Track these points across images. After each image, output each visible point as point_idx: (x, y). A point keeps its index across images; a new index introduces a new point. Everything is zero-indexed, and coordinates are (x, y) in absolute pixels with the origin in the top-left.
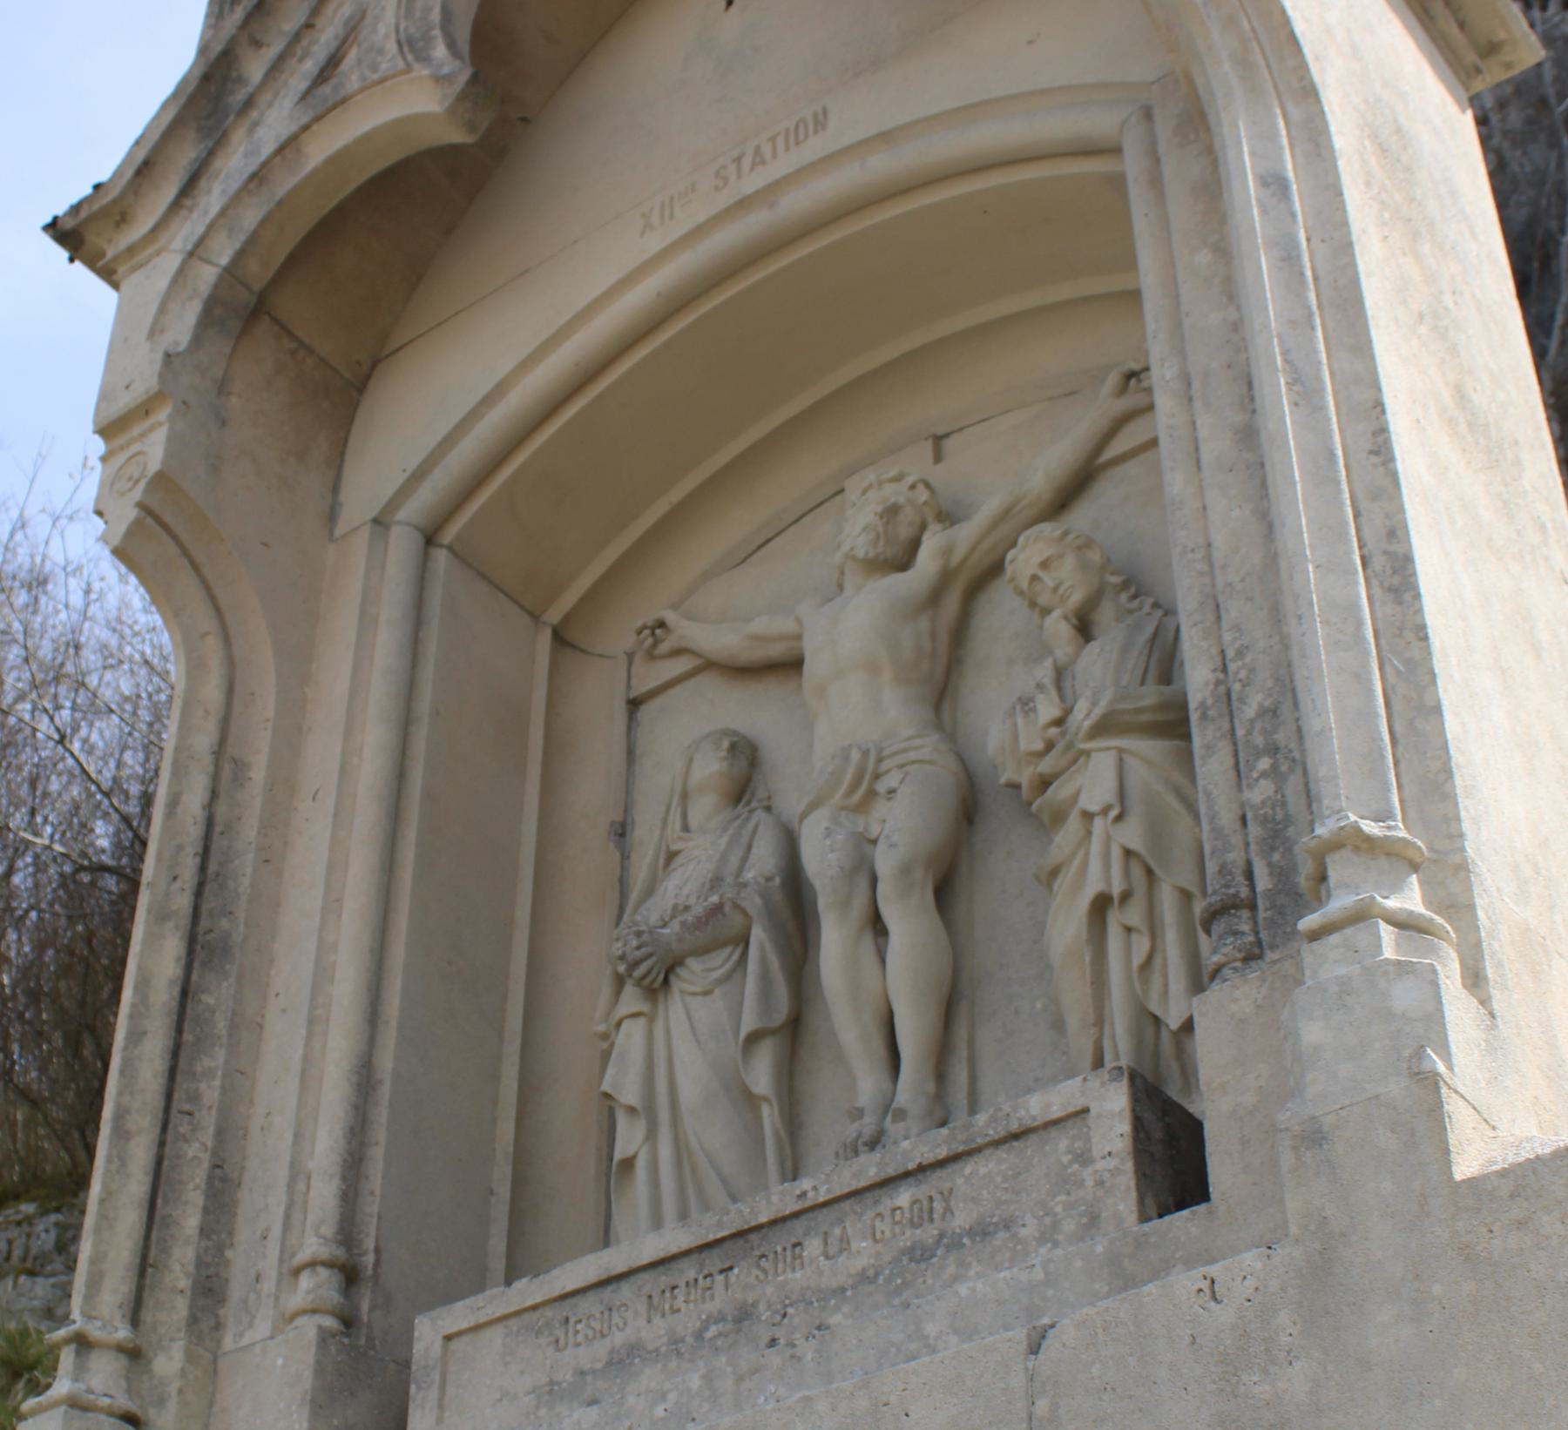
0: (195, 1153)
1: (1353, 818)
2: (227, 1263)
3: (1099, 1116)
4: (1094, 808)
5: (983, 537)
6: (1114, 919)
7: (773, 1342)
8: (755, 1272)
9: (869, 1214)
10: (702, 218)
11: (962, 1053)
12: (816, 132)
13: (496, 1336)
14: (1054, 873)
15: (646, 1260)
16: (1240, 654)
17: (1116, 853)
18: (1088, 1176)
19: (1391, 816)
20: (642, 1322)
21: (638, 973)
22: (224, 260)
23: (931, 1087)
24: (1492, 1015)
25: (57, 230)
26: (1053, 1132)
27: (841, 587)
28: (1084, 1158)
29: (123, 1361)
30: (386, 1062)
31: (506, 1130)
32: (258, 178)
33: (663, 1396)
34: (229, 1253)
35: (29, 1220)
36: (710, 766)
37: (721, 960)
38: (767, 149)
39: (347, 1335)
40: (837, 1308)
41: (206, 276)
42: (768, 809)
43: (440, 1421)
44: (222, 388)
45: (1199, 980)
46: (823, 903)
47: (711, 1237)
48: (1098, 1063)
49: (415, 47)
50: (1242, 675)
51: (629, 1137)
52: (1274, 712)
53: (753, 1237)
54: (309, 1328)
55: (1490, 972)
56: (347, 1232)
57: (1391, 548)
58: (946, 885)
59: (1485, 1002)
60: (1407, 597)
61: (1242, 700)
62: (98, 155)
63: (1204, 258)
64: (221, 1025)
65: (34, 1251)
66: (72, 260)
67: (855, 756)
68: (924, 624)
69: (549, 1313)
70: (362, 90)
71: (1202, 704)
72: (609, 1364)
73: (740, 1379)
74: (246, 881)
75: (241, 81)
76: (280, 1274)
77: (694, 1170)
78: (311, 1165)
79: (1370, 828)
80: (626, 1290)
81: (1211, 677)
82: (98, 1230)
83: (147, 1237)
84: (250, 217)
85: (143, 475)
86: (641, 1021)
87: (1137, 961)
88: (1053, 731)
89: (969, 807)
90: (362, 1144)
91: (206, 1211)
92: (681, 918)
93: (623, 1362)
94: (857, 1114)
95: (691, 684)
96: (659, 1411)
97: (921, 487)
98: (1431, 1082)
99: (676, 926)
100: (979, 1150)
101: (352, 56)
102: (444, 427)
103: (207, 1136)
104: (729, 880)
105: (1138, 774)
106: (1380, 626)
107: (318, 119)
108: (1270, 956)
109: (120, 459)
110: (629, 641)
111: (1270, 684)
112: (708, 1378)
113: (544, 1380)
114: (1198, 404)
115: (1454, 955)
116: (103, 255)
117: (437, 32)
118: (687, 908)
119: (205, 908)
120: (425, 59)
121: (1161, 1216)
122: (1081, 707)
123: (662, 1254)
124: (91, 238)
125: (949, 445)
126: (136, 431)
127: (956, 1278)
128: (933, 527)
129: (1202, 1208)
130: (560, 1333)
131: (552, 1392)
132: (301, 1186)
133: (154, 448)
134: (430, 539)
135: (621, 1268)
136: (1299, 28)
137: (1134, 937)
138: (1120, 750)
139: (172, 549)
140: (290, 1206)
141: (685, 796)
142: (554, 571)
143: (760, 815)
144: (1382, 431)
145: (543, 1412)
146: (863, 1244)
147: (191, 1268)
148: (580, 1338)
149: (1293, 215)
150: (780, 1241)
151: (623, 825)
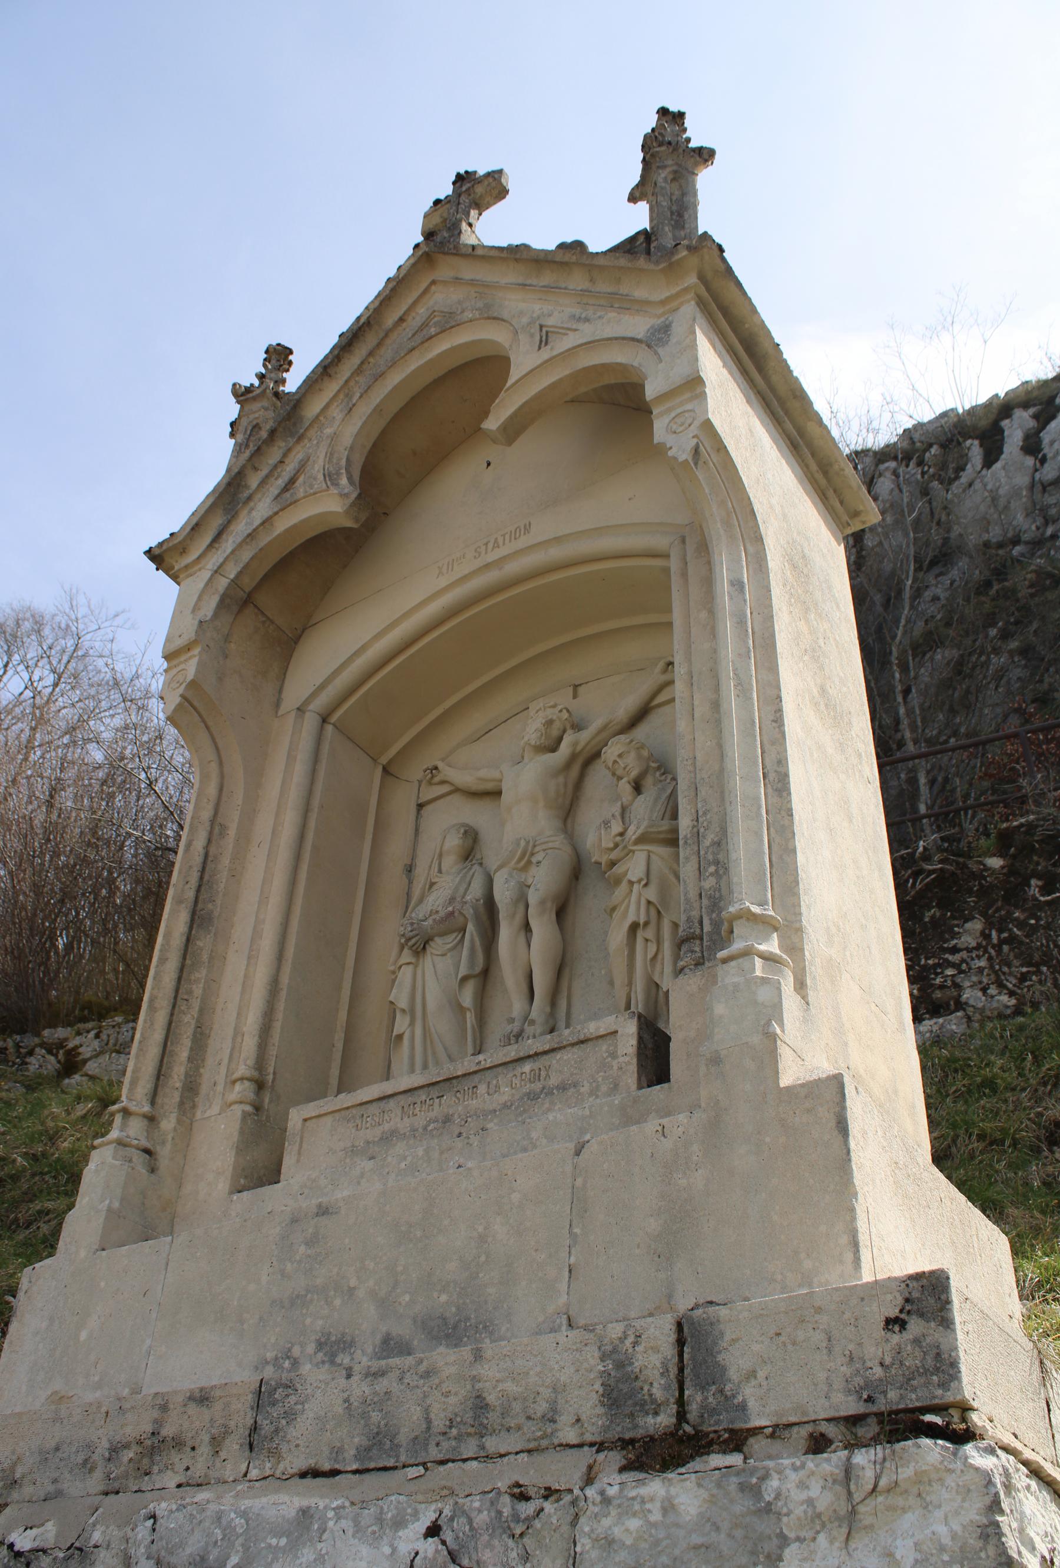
0: (188, 1021)
1: (747, 904)
2: (201, 1075)
3: (622, 1035)
4: (634, 879)
5: (593, 738)
6: (640, 934)
7: (460, 1135)
8: (454, 1099)
9: (510, 1075)
10: (466, 572)
11: (564, 994)
12: (14, 1297)
13: (328, 1120)
14: (614, 909)
15: (402, 1089)
16: (705, 814)
17: (643, 902)
18: (615, 1064)
19: (766, 903)
20: (398, 1119)
21: (410, 944)
22: (232, 576)
23: (548, 1009)
24: (808, 1004)
25: (151, 554)
26: (600, 1041)
27: (523, 757)
28: (613, 1055)
29: (146, 1122)
30: (285, 980)
31: (343, 1015)
32: (251, 536)
33: (405, 1158)
34: (202, 1070)
35: (119, 1025)
36: (454, 841)
37: (451, 939)
38: (500, 540)
39: (257, 1115)
40: (491, 1121)
41: (223, 583)
42: (481, 864)
43: (298, 1161)
44: (227, 639)
45: (679, 972)
46: (502, 915)
47: (434, 1080)
48: (628, 1007)
49: (331, 477)
50: (705, 824)
51: (401, 1024)
52: (719, 844)
53: (454, 1081)
54: (238, 1110)
55: (808, 982)
56: (260, 1063)
57: (779, 770)
58: (562, 911)
59: (804, 997)
60: (784, 794)
61: (704, 837)
62: (170, 518)
63: (704, 615)
64: (205, 957)
65: (120, 1041)
66: (157, 569)
67: (523, 843)
68: (561, 779)
69: (354, 1111)
70: (304, 497)
71: (685, 836)
72: (381, 1139)
73: (442, 1153)
74: (222, 886)
75: (247, 487)
76: (226, 1082)
77: (432, 1042)
78: (245, 1029)
79: (756, 909)
80: (392, 1103)
81: (691, 824)
82: (137, 1056)
83: (162, 1061)
84: (246, 555)
85: (184, 680)
86: (411, 967)
87: (650, 956)
88: (618, 838)
89: (577, 871)
90: (271, 1020)
91: (191, 1049)
92: (433, 917)
93: (388, 1138)
94: (511, 1020)
95: (448, 798)
96: (403, 1165)
97: (565, 711)
98: (773, 1038)
99: (430, 921)
100: (564, 1047)
101: (301, 479)
102: (335, 666)
103: (195, 1012)
104: (459, 899)
105: (657, 864)
106: (770, 808)
107: (282, 510)
108: (707, 964)
109: (174, 671)
110: (420, 775)
111: (718, 829)
112: (427, 1151)
113: (350, 1144)
114: (695, 687)
115: (791, 974)
116: (173, 568)
117: (343, 471)
118: (437, 912)
119: (201, 898)
120: (336, 485)
121: (649, 1086)
122: (632, 828)
123: (410, 1087)
124: (168, 559)
125: (581, 690)
126: (182, 658)
127: (549, 1110)
128: (569, 731)
129: (666, 1085)
130: (359, 1122)
131: (353, 1151)
132: (239, 1039)
133: (190, 668)
134: (324, 720)
135: (390, 1092)
136: (756, 507)
137: (649, 943)
138: (649, 852)
139: (197, 718)
140: (233, 1049)
141: (441, 855)
142: (383, 737)
143: (476, 867)
144: (780, 711)
145: (348, 1160)
146: (507, 1088)
147: (182, 1077)
148: (368, 1125)
149: (745, 601)
150: (467, 1084)
151: (411, 866)
